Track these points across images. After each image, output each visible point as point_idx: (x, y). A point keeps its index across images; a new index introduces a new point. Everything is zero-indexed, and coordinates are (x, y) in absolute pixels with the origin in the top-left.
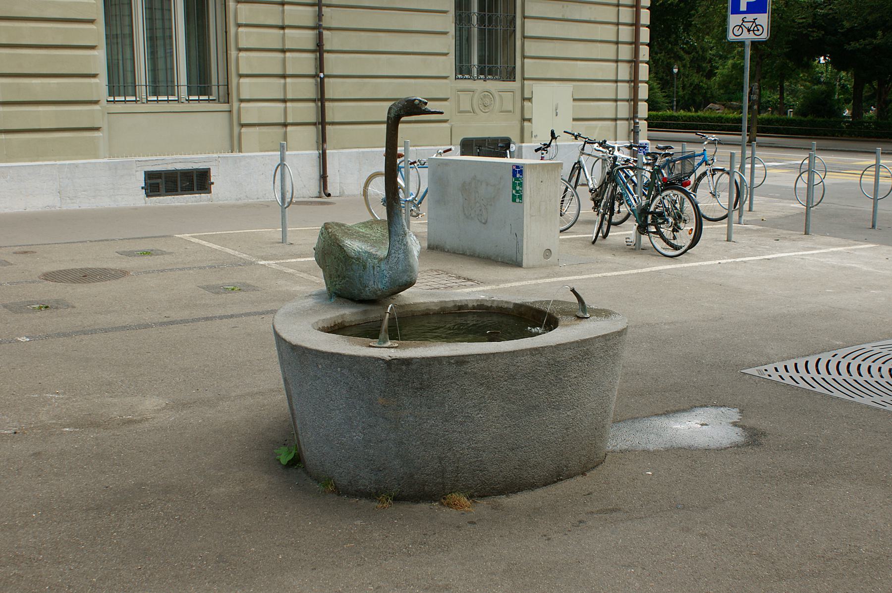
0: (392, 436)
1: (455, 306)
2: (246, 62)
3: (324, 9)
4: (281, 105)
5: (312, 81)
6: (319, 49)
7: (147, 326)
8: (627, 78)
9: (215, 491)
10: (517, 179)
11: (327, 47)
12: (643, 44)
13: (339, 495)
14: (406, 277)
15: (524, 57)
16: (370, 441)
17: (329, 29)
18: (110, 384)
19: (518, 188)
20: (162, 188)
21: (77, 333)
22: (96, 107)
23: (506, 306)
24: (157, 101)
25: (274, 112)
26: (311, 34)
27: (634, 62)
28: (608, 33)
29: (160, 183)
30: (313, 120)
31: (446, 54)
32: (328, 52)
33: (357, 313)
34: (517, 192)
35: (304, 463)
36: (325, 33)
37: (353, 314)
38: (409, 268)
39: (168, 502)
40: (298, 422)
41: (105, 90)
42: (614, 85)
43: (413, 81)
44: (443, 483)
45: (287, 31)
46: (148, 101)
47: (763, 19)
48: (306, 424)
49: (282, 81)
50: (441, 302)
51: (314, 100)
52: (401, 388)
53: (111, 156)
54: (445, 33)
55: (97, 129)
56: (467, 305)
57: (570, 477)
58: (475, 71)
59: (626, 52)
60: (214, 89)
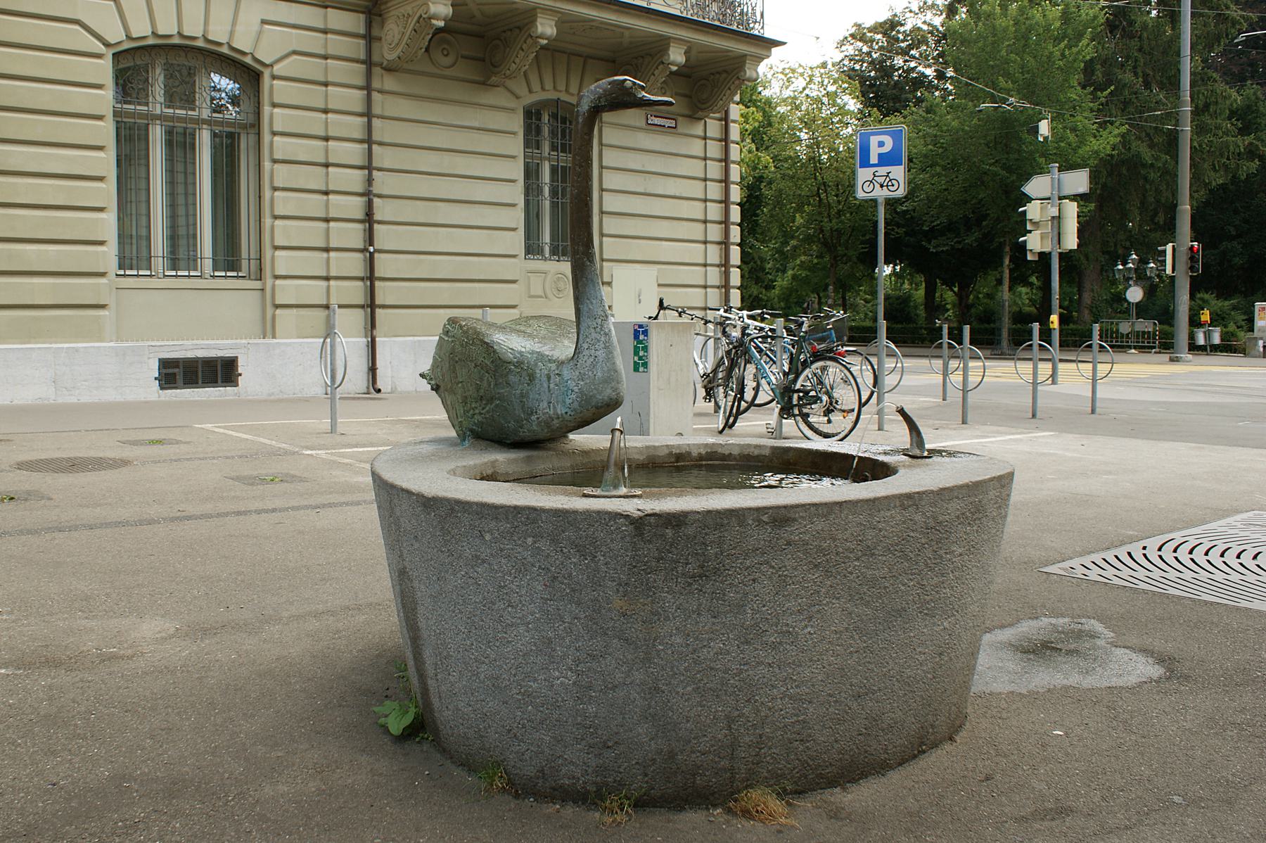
0: (638, 676)
1: (671, 453)
2: (283, 232)
3: (375, 173)
4: (324, 283)
5: (359, 256)
6: (369, 219)
7: (151, 522)
8: (718, 262)
9: (268, 790)
10: (641, 342)
11: (377, 217)
12: (734, 224)
13: (517, 796)
14: (609, 391)
15: (602, 235)
16: (590, 688)
17: (380, 196)
18: (87, 598)
19: (641, 353)
20: (180, 378)
21: (48, 530)
22: (103, 281)
23: (756, 452)
24: (176, 276)
25: (314, 291)
26: (359, 202)
27: (725, 244)
28: (696, 210)
29: (177, 373)
30: (361, 302)
31: (514, 230)
32: (379, 222)
33: (515, 460)
34: (640, 358)
35: (436, 731)
36: (376, 200)
37: (510, 462)
38: (612, 377)
39: (174, 817)
40: (427, 653)
41: (114, 262)
42: (703, 269)
43: (476, 259)
44: (732, 768)
45: (331, 197)
46: (165, 276)
47: (898, 172)
48: (448, 657)
49: (325, 255)
50: (647, 447)
51: (362, 279)
52: (662, 575)
53: (119, 339)
54: (514, 205)
55: (103, 307)
56: (689, 453)
57: (935, 745)
58: (547, 249)
59: (715, 232)
60: (244, 263)
